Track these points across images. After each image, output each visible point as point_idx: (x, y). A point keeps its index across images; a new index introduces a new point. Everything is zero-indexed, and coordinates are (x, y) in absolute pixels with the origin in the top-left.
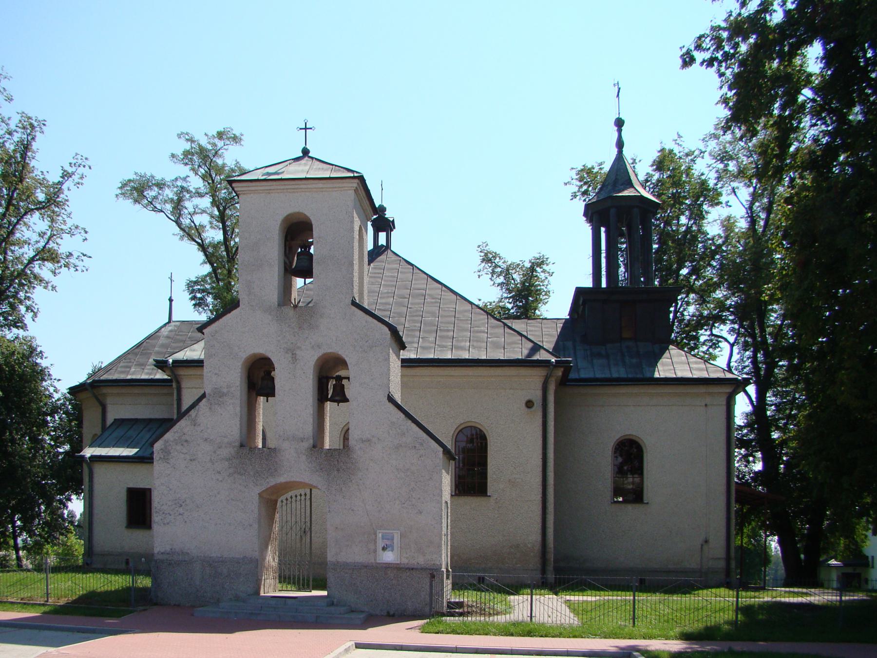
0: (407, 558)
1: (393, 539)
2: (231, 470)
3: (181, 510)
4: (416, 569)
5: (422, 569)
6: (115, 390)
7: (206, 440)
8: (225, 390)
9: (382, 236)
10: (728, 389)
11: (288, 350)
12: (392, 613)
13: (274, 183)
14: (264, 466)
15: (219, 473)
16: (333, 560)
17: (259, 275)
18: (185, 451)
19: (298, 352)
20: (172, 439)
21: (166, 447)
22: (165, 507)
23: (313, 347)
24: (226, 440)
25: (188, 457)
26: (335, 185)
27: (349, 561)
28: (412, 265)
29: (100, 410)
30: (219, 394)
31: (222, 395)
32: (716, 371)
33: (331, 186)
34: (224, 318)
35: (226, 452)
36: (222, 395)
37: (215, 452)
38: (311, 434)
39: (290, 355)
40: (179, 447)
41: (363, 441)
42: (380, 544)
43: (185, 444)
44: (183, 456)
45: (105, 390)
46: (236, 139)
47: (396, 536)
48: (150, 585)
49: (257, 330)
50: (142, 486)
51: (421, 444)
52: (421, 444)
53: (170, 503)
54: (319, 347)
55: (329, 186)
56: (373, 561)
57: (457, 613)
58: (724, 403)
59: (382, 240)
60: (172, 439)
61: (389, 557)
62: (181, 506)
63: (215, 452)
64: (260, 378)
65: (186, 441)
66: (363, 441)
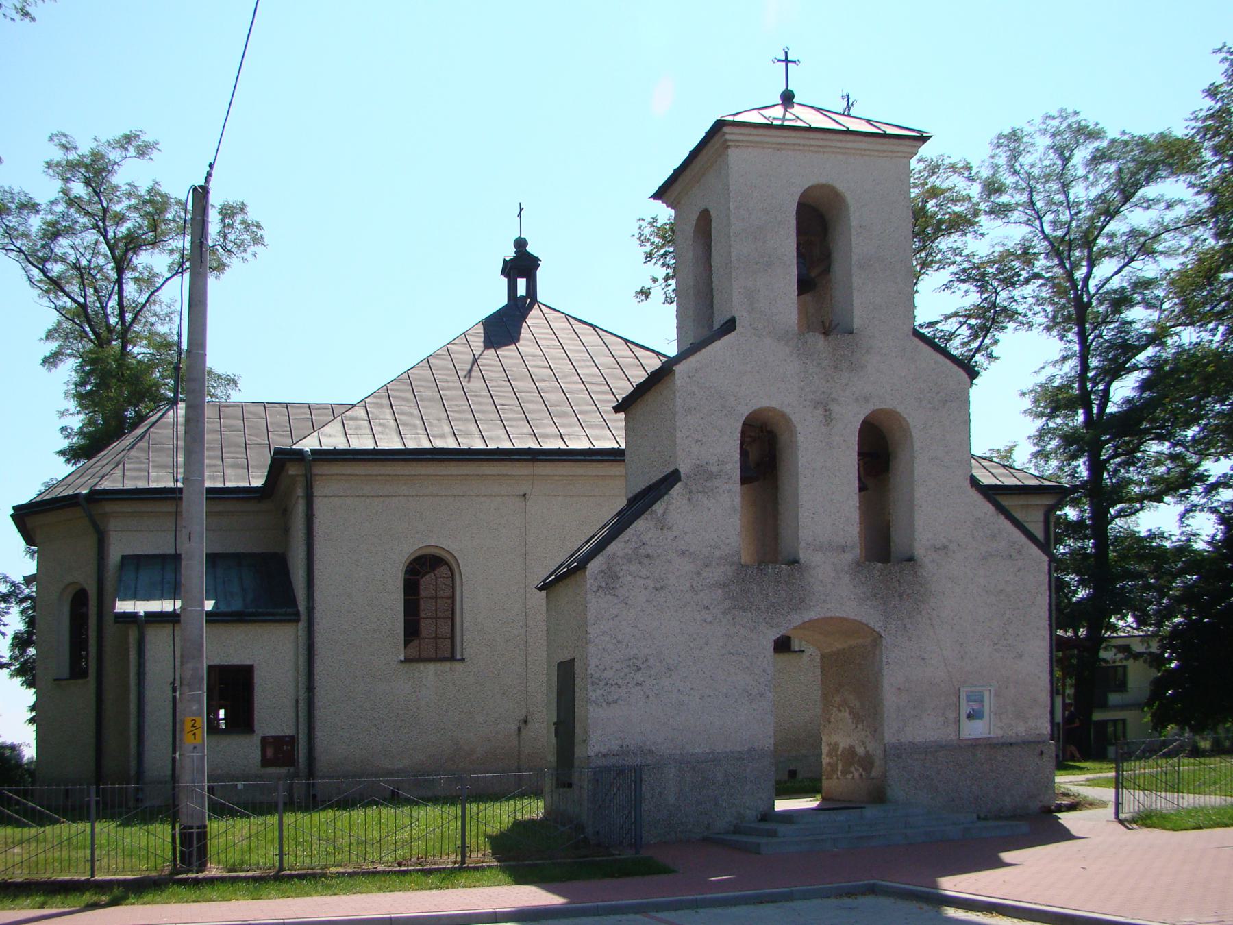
0: (1002, 728)
1: (982, 701)
2: (728, 604)
3: (639, 677)
4: (1017, 744)
5: (1024, 743)
6: (127, 508)
7: (683, 553)
8: (714, 469)
9: (522, 284)
10: (1048, 501)
11: (817, 404)
12: (982, 816)
13: (793, 134)
14: (783, 594)
15: (707, 608)
16: (893, 740)
17: (766, 282)
18: (644, 573)
19: (835, 408)
20: (621, 553)
21: (609, 568)
22: (606, 674)
23: (857, 400)
24: (718, 553)
25: (651, 584)
26: (885, 147)
27: (918, 739)
28: (594, 327)
29: (91, 541)
30: (705, 474)
31: (711, 476)
32: (1027, 478)
33: (879, 147)
34: (709, 348)
35: (717, 573)
36: (711, 476)
37: (699, 574)
38: (857, 539)
39: (820, 411)
40: (633, 568)
41: (936, 549)
42: (965, 709)
43: (646, 561)
44: (642, 582)
45: (109, 507)
46: (144, 150)
47: (986, 695)
48: (776, 802)
49: (762, 370)
50: (235, 661)
51: (1019, 552)
52: (1019, 552)
53: (618, 666)
54: (867, 399)
55: (879, 147)
56: (953, 737)
57: (1065, 805)
58: (1041, 518)
59: (522, 284)
60: (621, 553)
61: (974, 730)
62: (639, 669)
63: (699, 574)
64: (763, 452)
65: (648, 556)
66: (936, 549)
